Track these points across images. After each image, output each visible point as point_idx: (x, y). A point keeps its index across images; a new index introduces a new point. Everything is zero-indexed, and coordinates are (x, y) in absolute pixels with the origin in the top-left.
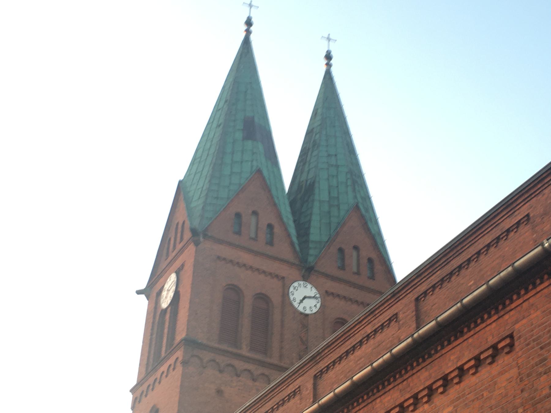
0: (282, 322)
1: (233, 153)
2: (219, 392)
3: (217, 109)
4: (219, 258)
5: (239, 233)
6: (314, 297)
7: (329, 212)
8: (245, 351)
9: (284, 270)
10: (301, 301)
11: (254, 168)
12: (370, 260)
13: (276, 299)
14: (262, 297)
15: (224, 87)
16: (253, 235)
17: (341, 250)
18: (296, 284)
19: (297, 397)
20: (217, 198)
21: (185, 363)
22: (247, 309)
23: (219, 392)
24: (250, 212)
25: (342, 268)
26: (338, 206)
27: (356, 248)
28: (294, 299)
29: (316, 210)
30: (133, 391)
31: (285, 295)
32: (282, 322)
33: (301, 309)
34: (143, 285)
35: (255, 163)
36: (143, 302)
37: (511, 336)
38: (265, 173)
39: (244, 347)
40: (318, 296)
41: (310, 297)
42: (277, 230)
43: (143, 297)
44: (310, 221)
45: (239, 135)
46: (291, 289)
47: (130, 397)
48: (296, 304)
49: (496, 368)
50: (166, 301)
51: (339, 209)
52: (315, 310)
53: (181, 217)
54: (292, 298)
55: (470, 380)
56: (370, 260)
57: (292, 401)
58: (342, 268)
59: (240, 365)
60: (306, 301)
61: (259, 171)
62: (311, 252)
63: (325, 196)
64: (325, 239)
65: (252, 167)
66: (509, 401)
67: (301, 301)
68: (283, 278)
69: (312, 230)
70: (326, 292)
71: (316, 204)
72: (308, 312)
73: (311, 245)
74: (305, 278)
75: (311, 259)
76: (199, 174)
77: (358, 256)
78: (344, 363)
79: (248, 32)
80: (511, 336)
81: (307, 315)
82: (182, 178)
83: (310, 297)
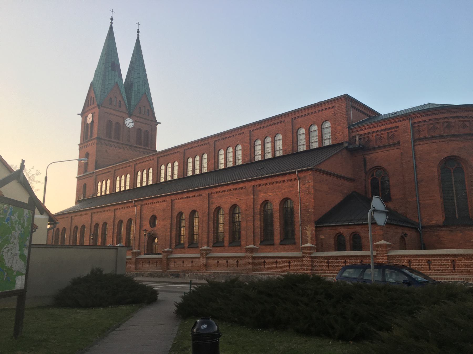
2: (106, 151)
3: (102, 56)
4: (105, 112)
5: (111, 104)
6: (132, 122)
8: (113, 140)
10: (128, 124)
11: (115, 82)
12: (148, 110)
14: (118, 123)
15: (104, 46)
16: (115, 104)
17: (140, 108)
18: (127, 119)
19: (130, 167)
20: (104, 93)
21: (97, 144)
23: (106, 151)
25: (140, 113)
28: (126, 124)
29: (133, 94)
30: (79, 145)
33: (128, 127)
34: (80, 112)
36: (80, 118)
38: (118, 83)
39: (113, 138)
41: (131, 123)
43: (80, 116)
44: (131, 97)
45: (110, 68)
46: (126, 121)
47: (78, 147)
48: (127, 125)
49: (164, 203)
50: (89, 121)
51: (140, 94)
52: (132, 126)
53: (93, 95)
55: (161, 203)
56: (148, 110)
57: (129, 167)
58: (140, 113)
59: (112, 143)
60: (130, 124)
61: (117, 83)
63: (136, 89)
65: (115, 81)
67: (128, 124)
68: (123, 117)
70: (135, 121)
71: (133, 91)
72: (130, 127)
74: (130, 117)
75: (131, 111)
76: (98, 82)
77: (145, 109)
78: (142, 164)
79: (112, 23)
81: (130, 128)
82: (92, 81)
83: (131, 123)
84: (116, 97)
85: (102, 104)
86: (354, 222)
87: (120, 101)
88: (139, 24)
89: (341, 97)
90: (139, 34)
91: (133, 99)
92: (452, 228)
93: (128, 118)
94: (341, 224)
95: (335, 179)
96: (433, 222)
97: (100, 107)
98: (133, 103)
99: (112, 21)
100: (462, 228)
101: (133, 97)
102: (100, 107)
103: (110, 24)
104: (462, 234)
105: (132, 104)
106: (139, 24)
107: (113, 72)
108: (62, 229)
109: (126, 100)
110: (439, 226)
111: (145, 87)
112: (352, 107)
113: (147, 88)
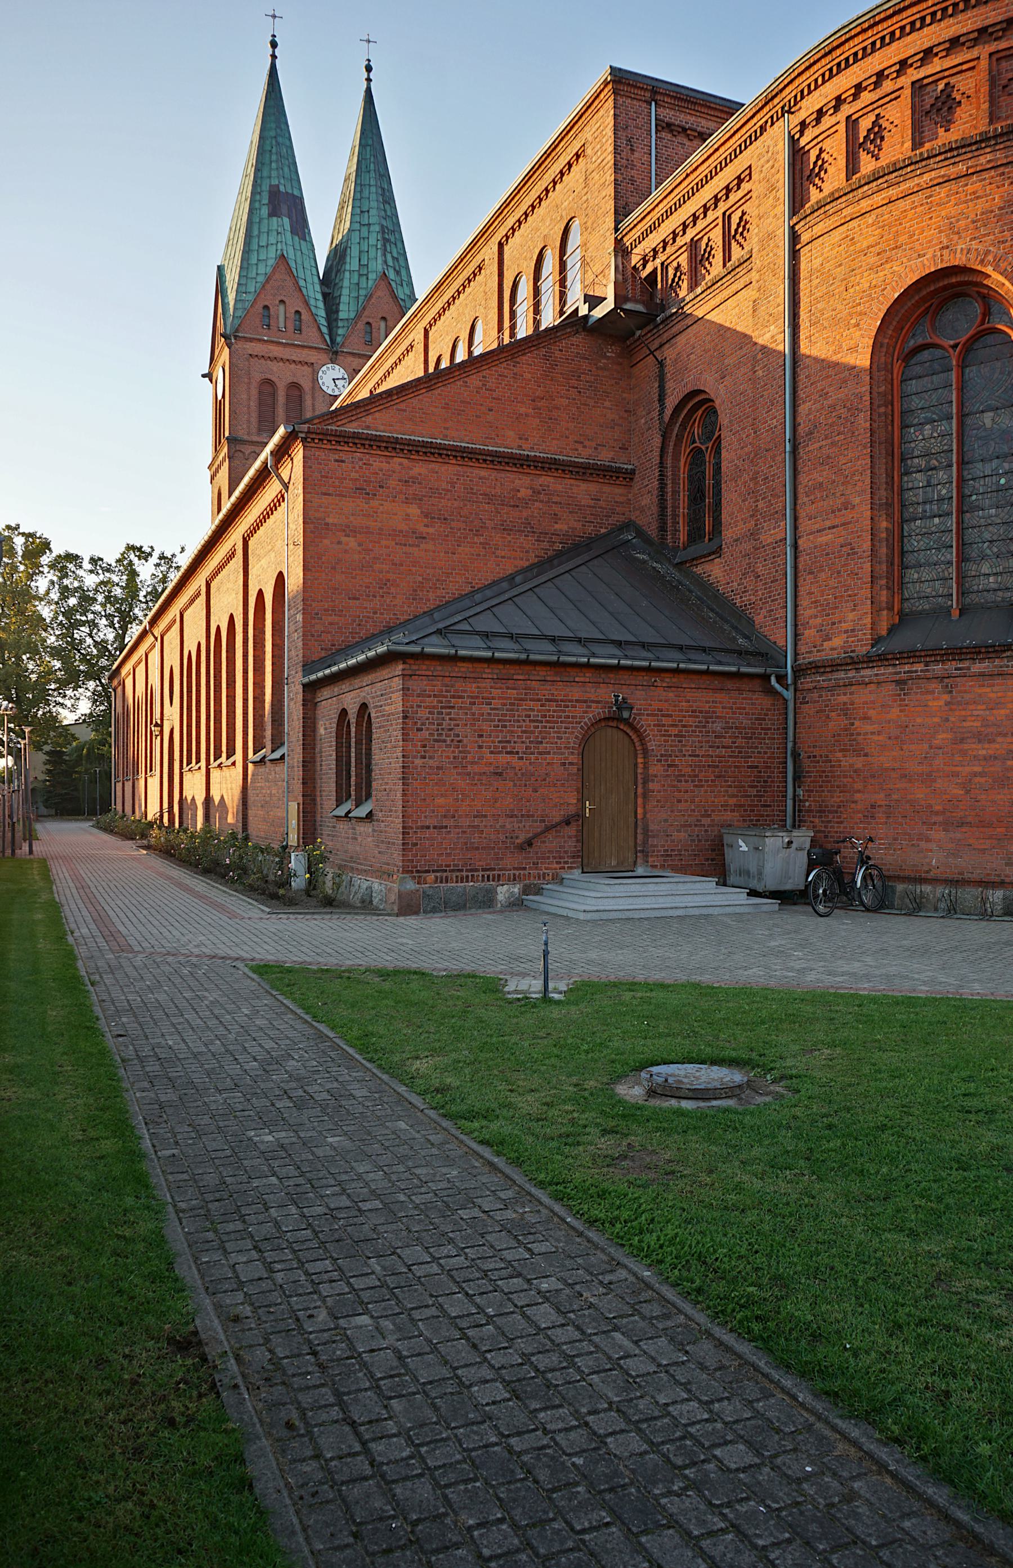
0: (313, 405)
1: (259, 237)
7: (358, 284)
9: (312, 357)
13: (306, 384)
14: (295, 386)
18: (324, 368)
22: (281, 399)
24: (277, 302)
26: (367, 275)
27: (384, 318)
29: (346, 283)
31: (315, 380)
32: (313, 405)
35: (279, 246)
37: (750, 167)
40: (346, 376)
42: (305, 316)
46: (320, 373)
54: (320, 382)
62: (340, 331)
63: (355, 266)
64: (352, 315)
66: (161, 875)
69: (342, 307)
71: (347, 274)
73: (340, 324)
75: (339, 339)
80: (750, 167)
84: (282, 302)
85: (237, 331)
86: (644, 660)
87: (297, 312)
88: (274, 16)
89: (699, 96)
90: (366, 76)
91: (344, 299)
92: (907, 668)
93: (329, 366)
94: (733, 669)
95: (483, 473)
96: (836, 645)
97: (233, 341)
98: (345, 312)
99: (274, 52)
100: (954, 664)
101: (345, 292)
102: (233, 341)
103: (270, 58)
104: (947, 697)
105: (342, 315)
106: (274, 16)
107: (275, 219)
108: (356, 710)
109: (321, 304)
110: (854, 663)
111: (384, 255)
112: (664, 126)
113: (395, 255)
